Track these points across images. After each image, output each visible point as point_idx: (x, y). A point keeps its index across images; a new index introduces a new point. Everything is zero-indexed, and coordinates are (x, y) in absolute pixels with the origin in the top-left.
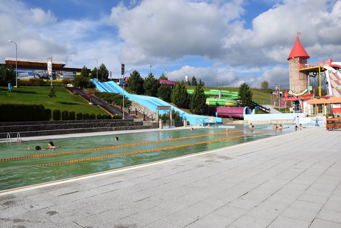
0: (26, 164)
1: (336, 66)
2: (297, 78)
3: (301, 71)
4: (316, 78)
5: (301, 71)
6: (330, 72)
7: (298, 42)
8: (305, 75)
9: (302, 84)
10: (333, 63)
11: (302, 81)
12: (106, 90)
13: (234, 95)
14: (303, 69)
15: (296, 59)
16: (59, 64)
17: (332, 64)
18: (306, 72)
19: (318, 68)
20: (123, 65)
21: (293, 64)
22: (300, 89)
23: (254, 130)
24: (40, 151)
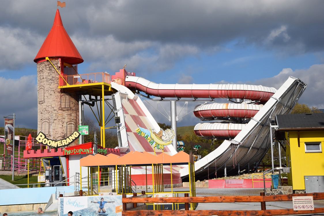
2: (55, 105)
4: (94, 108)
6: (123, 96)
7: (58, 25)
8: (73, 100)
9: (66, 120)
10: (130, 79)
11: (65, 114)
14: (68, 86)
15: (54, 62)
17: (127, 80)
18: (76, 94)
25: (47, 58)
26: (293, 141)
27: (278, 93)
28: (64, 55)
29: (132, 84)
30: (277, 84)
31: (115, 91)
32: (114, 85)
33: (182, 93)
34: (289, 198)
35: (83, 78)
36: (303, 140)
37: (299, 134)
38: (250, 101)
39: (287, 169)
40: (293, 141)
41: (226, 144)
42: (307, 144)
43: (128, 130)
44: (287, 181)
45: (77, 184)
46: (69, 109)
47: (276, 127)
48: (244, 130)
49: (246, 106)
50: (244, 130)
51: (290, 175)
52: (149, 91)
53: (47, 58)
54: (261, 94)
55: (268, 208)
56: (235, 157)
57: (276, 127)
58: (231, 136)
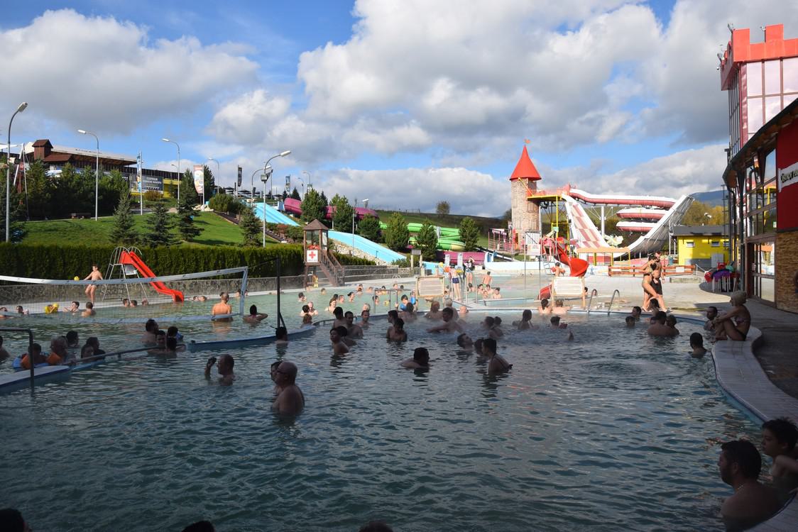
0: (181, 368)
1: (651, 202)
2: (525, 209)
3: (529, 200)
4: (547, 210)
5: (529, 200)
6: (571, 204)
7: (525, 155)
8: (536, 206)
9: (531, 219)
10: (573, 191)
11: (531, 214)
12: (273, 219)
13: (453, 234)
14: (533, 197)
15: (523, 181)
16: (105, 157)
17: (571, 192)
18: (537, 202)
19: (555, 198)
20: (240, 169)
21: (518, 188)
22: (527, 226)
23: (620, 270)
24: (593, 276)
25: (519, 178)
26: (680, 241)
27: (678, 203)
28: (531, 176)
29: (574, 195)
30: (677, 198)
31: (564, 200)
32: (564, 196)
33: (610, 201)
34: (675, 268)
35: (542, 189)
36: (685, 241)
37: (684, 238)
38: (656, 207)
39: (675, 255)
40: (680, 241)
41: (641, 239)
42: (688, 243)
43: (576, 227)
44: (676, 262)
45: (636, 271)
46: (533, 211)
47: (672, 234)
48: (654, 228)
49: (653, 211)
50: (654, 228)
51: (678, 258)
52: (586, 199)
53: (519, 178)
54: (664, 203)
55: (25, 310)
56: (646, 247)
57: (672, 234)
58: (645, 232)
